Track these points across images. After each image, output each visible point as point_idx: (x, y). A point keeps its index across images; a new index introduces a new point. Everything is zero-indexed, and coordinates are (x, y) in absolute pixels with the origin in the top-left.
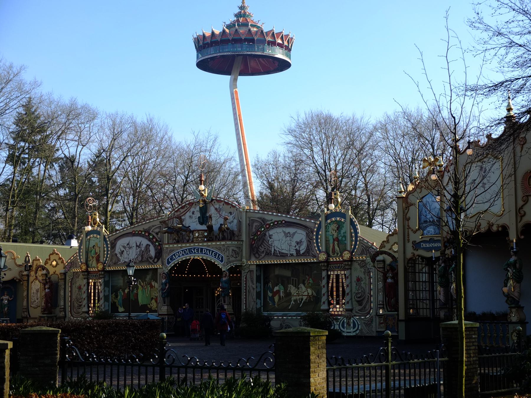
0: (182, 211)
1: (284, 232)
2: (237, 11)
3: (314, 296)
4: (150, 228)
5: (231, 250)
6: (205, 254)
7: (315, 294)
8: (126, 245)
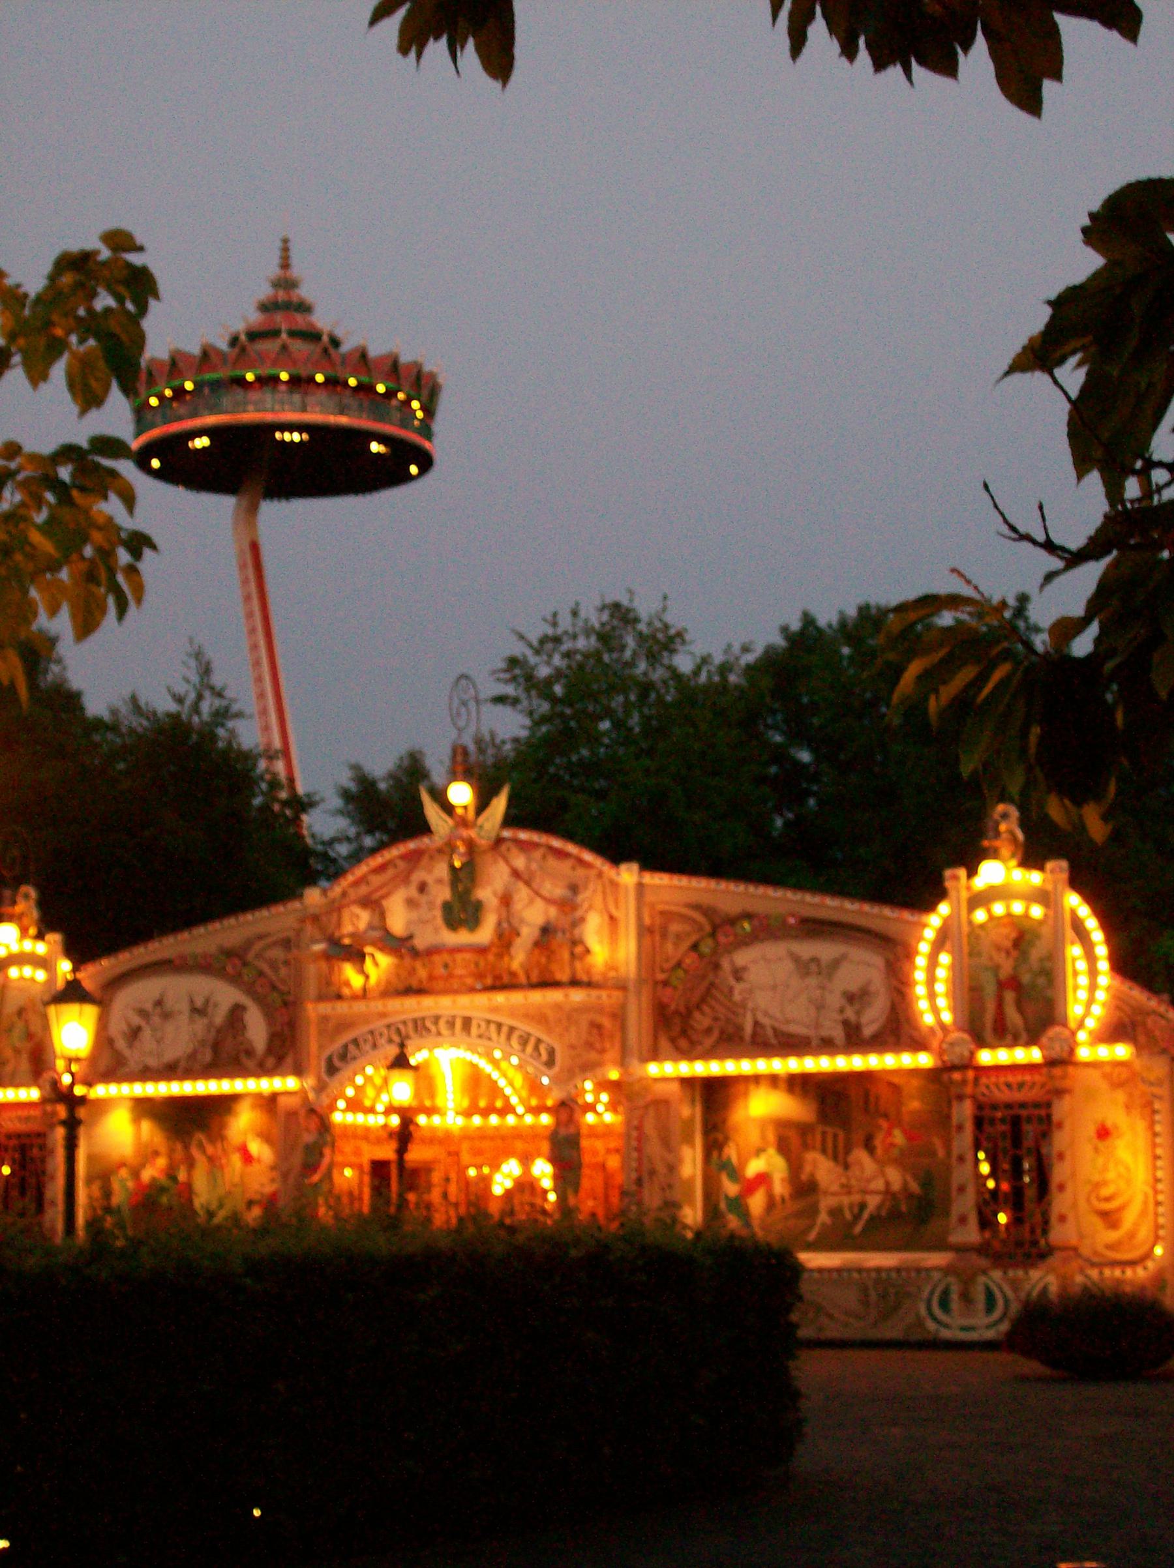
0: (376, 880)
1: (796, 959)
2: (265, 291)
3: (910, 1196)
4: (249, 944)
5: (584, 1025)
6: (480, 1036)
7: (914, 1187)
8: (148, 1006)
